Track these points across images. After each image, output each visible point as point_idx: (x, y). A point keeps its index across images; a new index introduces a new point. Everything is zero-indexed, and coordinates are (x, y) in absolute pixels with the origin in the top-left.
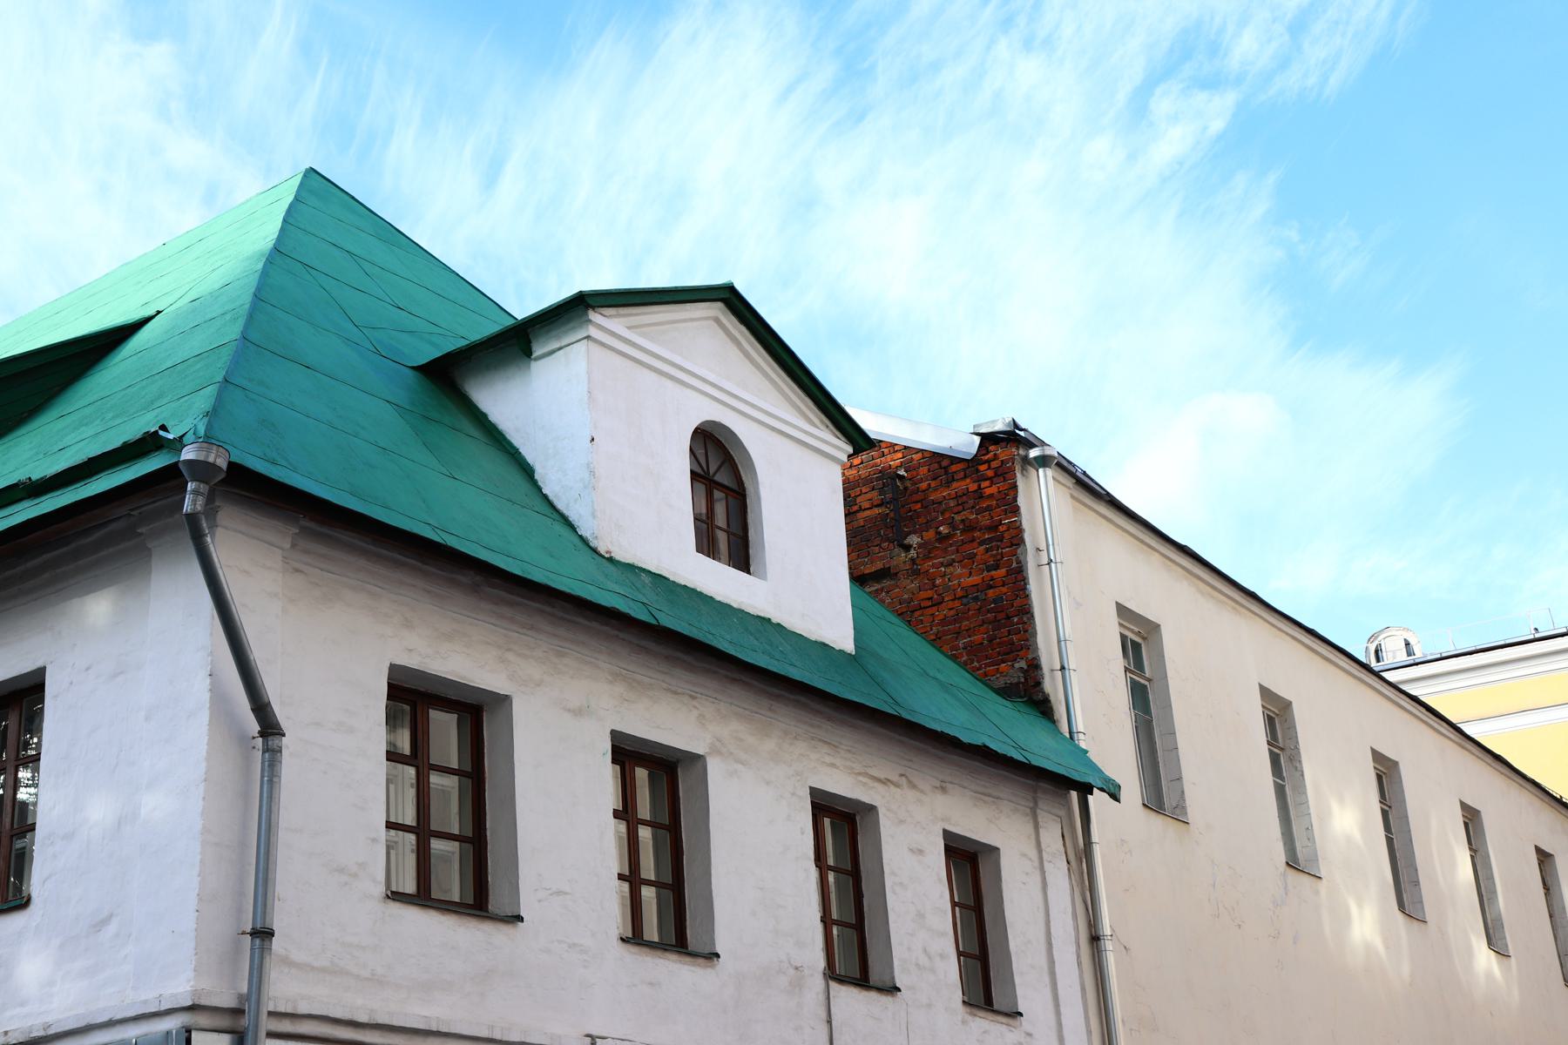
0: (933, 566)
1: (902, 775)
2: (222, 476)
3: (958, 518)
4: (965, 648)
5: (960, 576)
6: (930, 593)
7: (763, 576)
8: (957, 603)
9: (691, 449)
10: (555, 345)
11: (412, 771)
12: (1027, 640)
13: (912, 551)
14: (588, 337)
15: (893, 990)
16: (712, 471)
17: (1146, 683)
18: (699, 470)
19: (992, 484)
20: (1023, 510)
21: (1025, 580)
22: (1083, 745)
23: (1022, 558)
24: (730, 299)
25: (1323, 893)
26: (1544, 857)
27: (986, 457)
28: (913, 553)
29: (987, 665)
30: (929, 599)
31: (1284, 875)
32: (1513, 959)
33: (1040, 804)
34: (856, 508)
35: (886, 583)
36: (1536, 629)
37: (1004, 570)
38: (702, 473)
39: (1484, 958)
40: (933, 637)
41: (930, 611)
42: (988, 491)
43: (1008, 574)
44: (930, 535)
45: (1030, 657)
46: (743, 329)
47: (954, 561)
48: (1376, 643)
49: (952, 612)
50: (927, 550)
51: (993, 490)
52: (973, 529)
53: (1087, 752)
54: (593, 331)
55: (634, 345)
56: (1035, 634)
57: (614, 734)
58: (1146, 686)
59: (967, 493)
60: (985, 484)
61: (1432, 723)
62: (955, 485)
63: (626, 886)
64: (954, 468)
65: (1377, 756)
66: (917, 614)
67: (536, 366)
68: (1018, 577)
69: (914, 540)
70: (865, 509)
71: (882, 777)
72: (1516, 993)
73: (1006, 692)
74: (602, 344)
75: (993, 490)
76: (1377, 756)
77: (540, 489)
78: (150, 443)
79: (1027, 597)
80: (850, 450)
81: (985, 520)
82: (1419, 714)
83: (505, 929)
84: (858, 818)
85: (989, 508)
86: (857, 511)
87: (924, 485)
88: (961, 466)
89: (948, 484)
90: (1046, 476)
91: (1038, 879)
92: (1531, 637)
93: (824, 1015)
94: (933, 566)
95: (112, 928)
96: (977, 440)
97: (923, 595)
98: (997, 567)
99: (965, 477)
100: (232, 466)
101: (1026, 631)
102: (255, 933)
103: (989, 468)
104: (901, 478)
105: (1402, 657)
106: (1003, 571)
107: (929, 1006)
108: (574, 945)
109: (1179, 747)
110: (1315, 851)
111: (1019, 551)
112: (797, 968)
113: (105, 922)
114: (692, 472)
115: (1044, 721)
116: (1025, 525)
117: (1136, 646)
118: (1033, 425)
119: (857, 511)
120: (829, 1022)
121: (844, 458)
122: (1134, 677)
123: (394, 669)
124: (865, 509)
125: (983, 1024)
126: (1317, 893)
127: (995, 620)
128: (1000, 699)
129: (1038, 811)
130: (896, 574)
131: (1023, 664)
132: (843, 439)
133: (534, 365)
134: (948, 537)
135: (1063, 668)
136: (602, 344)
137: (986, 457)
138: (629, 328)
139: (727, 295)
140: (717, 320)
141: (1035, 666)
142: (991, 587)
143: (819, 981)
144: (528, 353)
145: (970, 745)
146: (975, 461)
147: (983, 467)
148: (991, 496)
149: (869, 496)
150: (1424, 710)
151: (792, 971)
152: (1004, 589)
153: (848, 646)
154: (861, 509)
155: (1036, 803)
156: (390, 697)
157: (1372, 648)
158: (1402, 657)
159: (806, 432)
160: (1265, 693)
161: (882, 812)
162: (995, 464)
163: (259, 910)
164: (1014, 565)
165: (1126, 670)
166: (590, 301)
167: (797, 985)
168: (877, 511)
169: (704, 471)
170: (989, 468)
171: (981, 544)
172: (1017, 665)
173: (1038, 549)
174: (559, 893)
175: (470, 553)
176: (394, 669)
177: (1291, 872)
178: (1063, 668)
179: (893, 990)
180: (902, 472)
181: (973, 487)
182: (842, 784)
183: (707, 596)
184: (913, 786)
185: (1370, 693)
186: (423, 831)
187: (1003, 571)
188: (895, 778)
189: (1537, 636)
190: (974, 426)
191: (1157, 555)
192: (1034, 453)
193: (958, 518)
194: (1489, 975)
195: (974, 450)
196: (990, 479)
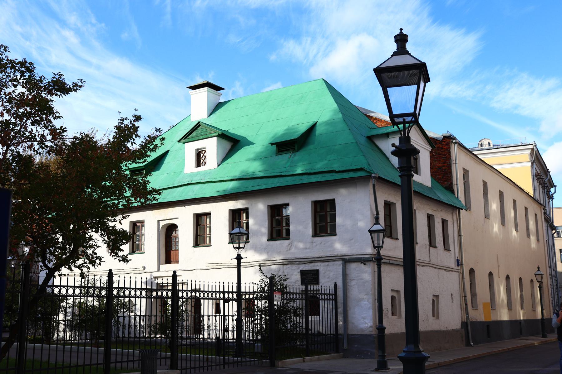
3: (437, 152)
5: (437, 164)
7: (420, 175)
12: (450, 178)
15: (436, 247)
20: (451, 152)
22: (460, 200)
23: (450, 162)
25: (490, 222)
26: (526, 208)
27: (444, 141)
29: (442, 182)
31: (484, 219)
32: (519, 232)
33: (454, 211)
36: (522, 143)
39: (514, 232)
42: (444, 147)
43: (448, 164)
46: (418, 129)
47: (436, 160)
48: (481, 142)
51: (445, 147)
52: (441, 155)
53: (461, 201)
59: (439, 147)
60: (443, 146)
61: (509, 181)
62: (437, 145)
64: (437, 142)
65: (500, 191)
67: (389, 139)
68: (450, 166)
72: (519, 239)
73: (446, 188)
75: (445, 147)
76: (500, 191)
77: (391, 162)
82: (509, 181)
83: (395, 241)
84: (430, 217)
85: (444, 151)
88: (438, 142)
90: (456, 146)
91: (452, 226)
92: (521, 145)
93: (429, 252)
95: (353, 241)
96: (442, 137)
98: (445, 163)
99: (439, 144)
105: (487, 147)
106: (446, 164)
107: (440, 250)
110: (489, 213)
113: (352, 239)
116: (451, 155)
118: (455, 134)
120: (430, 253)
123: (385, 200)
125: (446, 252)
126: (489, 222)
128: (445, 190)
129: (454, 213)
131: (449, 183)
134: (435, 155)
135: (457, 184)
143: (428, 247)
145: (449, 204)
147: (443, 142)
148: (445, 149)
150: (508, 180)
153: (430, 186)
155: (453, 212)
157: (480, 143)
158: (487, 147)
160: (483, 181)
161: (435, 216)
162: (446, 142)
164: (449, 163)
167: (426, 248)
170: (445, 143)
171: (442, 158)
172: (448, 183)
175: (215, 84)
176: (385, 200)
177: (485, 218)
179: (436, 247)
181: (441, 146)
182: (430, 212)
183: (418, 183)
184: (438, 211)
185: (501, 178)
187: (446, 164)
188: (436, 210)
189: (522, 144)
190: (442, 134)
191: (469, 156)
192: (454, 141)
193: (437, 152)
194: (515, 236)
195: (442, 139)
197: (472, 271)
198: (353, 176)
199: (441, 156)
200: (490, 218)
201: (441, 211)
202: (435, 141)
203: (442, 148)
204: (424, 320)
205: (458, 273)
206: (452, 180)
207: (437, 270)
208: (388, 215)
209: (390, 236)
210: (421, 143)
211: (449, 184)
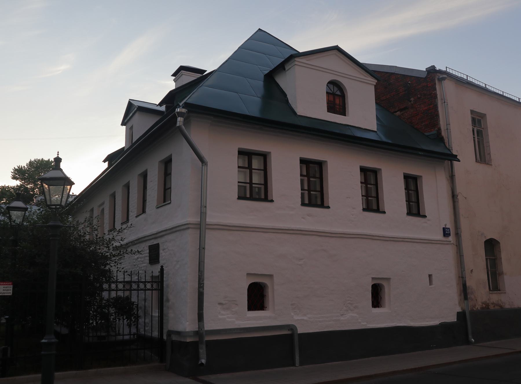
10: (290, 66)
13: (412, 102)
14: (295, 65)
16: (335, 92)
17: (482, 129)
18: (329, 91)
24: (337, 49)
27: (429, 76)
30: (416, 114)
34: (399, 92)
37: (433, 105)
38: (331, 92)
54: (296, 63)
55: (308, 64)
56: (440, 121)
58: (482, 130)
70: (402, 92)
74: (300, 66)
79: (438, 112)
80: (376, 81)
86: (400, 93)
100: (123, 124)
109: (490, 145)
111: (436, 100)
119: (400, 93)
122: (477, 128)
124: (402, 92)
132: (374, 79)
133: (287, 72)
136: (300, 66)
137: (429, 76)
138: (307, 60)
141: (439, 129)
144: (285, 69)
159: (365, 79)
169: (332, 91)
173: (442, 99)
178: (447, 129)
209: (417, 213)
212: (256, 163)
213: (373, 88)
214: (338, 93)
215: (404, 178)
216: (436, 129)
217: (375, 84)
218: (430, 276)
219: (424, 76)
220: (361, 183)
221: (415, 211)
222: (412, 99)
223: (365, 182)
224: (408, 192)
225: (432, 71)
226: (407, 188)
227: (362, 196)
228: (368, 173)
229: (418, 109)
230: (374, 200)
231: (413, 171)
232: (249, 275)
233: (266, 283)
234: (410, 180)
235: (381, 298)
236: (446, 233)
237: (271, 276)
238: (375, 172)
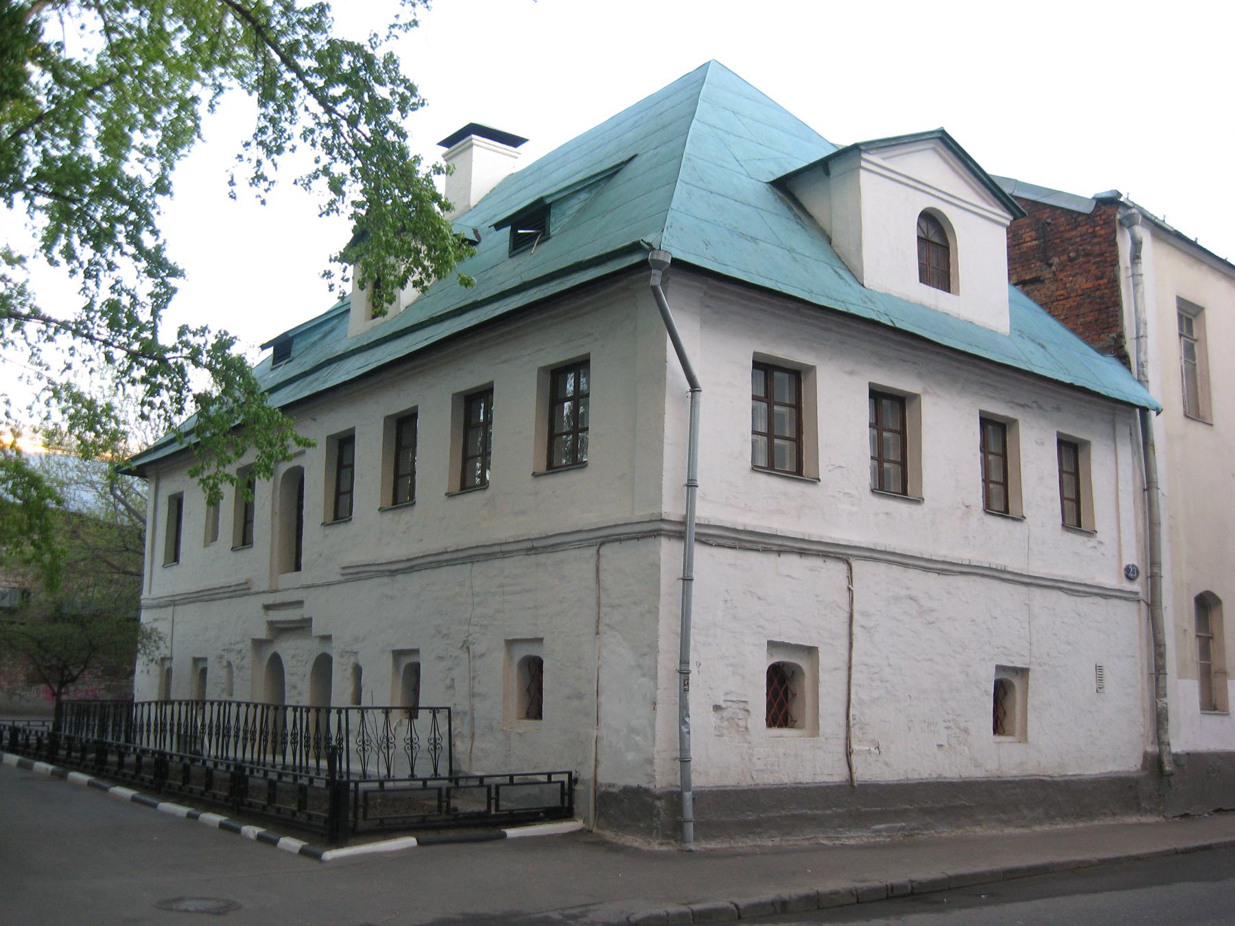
0: (1065, 276)
1: (1035, 402)
2: (667, 266)
3: (1081, 248)
4: (1081, 325)
6: (1062, 292)
8: (1078, 298)
9: (918, 223)
11: (764, 405)
18: (923, 236)
19: (1102, 229)
21: (1118, 286)
24: (943, 140)
27: (1098, 213)
28: (1054, 268)
30: (1062, 295)
35: (1039, 286)
40: (1062, 317)
41: (1064, 302)
43: (1108, 282)
44: (1065, 257)
45: (1119, 330)
47: (1077, 274)
49: (1075, 304)
50: (1062, 267)
51: (1103, 232)
57: (870, 383)
60: (1098, 228)
62: (1079, 229)
63: (876, 463)
64: (1080, 219)
66: (1055, 304)
69: (1056, 260)
71: (1022, 403)
73: (1103, 351)
78: (635, 247)
80: (1012, 218)
81: (1096, 249)
87: (1062, 229)
89: (1076, 228)
94: (1065, 276)
97: (1059, 293)
98: (1102, 278)
101: (1117, 316)
102: (688, 486)
103: (1100, 219)
104: (1049, 224)
106: (1105, 281)
108: (848, 493)
112: (967, 507)
114: (918, 237)
115: (1128, 371)
117: (1028, 605)
119: (1021, 243)
121: (1008, 223)
123: (755, 354)
125: (1076, 540)
127: (1100, 310)
130: (1044, 280)
131: (1114, 335)
138: (883, 159)
139: (940, 135)
140: (934, 149)
141: (1121, 336)
142: (1098, 290)
146: (1089, 217)
149: (1029, 234)
151: (964, 508)
152: (1106, 291)
154: (1025, 242)
155: (1114, 429)
156: (754, 367)
162: (1103, 217)
163: (972, 165)
165: (1181, 335)
166: (862, 148)
168: (1034, 243)
170: (1100, 219)
174: (840, 467)
180: (1049, 221)
182: (999, 409)
184: (1040, 407)
186: (770, 435)
187: (1105, 281)
196: (1100, 225)
197: (1206, 604)
198: (618, 268)
199: (1091, 258)
200: (1214, 422)
201: (1058, 409)
202: (1075, 219)
203: (1094, 235)
204: (945, 743)
205: (1132, 607)
206: (1122, 326)
207: (1024, 589)
208: (1070, 473)
209: (1003, 510)
210: (975, 203)
211: (1113, 338)
212: (784, 390)
213: (1003, 233)
214: (936, 239)
215: (870, 397)
216: (1114, 335)
217: (1008, 223)
218: (1099, 669)
219: (1088, 209)
220: (754, 398)
221: (998, 505)
222: (1056, 260)
223: (765, 396)
224: (880, 436)
225: (1110, 204)
226: (877, 424)
227: (754, 432)
228: (777, 374)
229: (1068, 285)
230: (787, 446)
231: (1075, 432)
232: (772, 645)
233: (803, 667)
234: (885, 402)
235: (1005, 713)
236: (1130, 573)
237: (811, 651)
238: (798, 375)
